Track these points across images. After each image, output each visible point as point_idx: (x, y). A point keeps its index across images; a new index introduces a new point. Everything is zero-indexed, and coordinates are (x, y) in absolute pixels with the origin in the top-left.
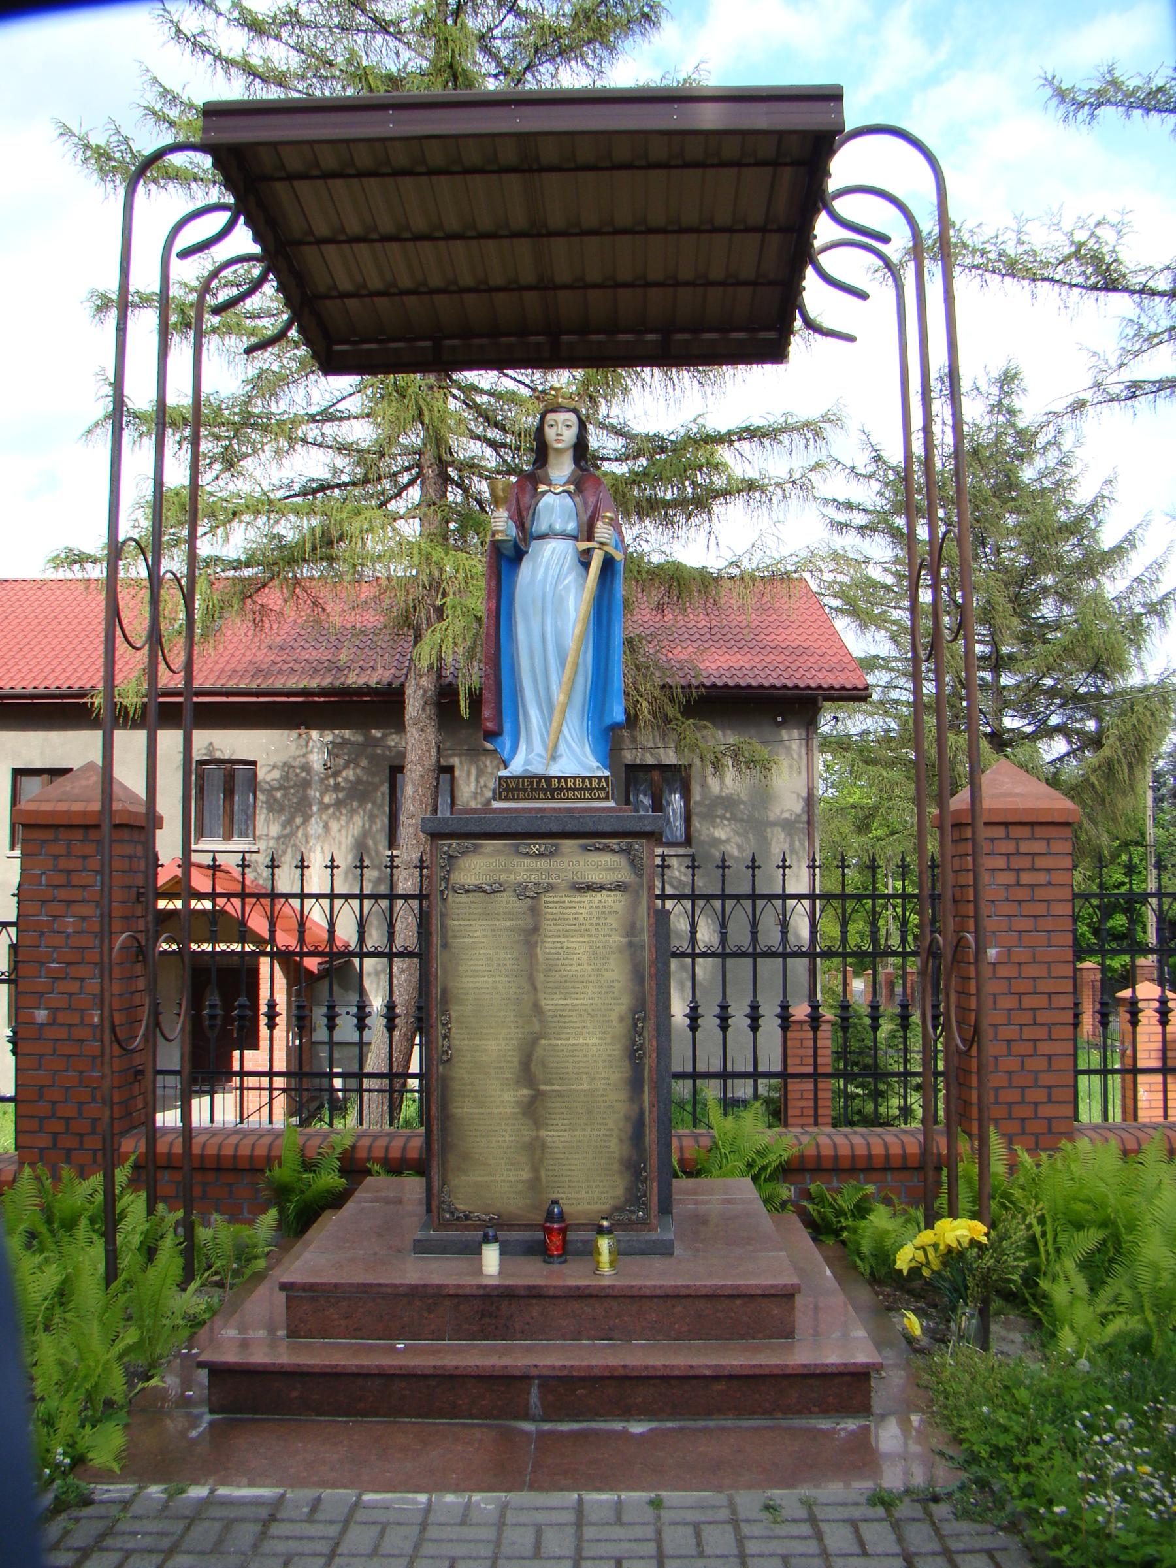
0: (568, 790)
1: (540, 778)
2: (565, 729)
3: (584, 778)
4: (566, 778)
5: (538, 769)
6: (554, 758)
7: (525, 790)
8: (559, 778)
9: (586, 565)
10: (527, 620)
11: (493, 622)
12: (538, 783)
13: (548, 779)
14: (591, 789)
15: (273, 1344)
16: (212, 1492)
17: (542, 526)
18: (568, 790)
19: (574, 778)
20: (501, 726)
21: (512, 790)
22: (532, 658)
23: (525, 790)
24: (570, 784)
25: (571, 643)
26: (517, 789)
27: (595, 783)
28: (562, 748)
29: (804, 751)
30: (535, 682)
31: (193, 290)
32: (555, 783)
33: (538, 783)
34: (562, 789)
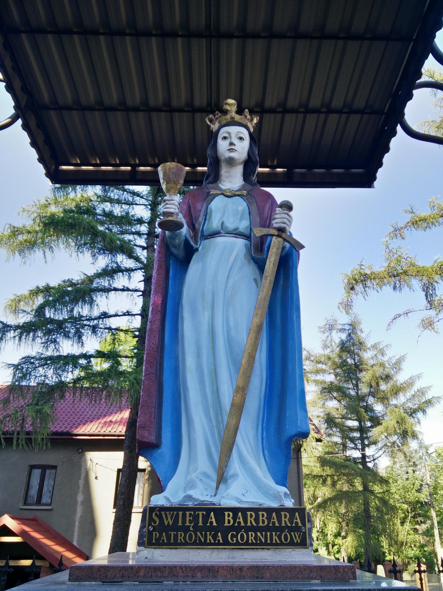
0: (248, 529)
1: (209, 510)
2: (239, 439)
3: (269, 511)
4: (244, 511)
5: (202, 494)
6: (222, 478)
7: (185, 529)
8: (235, 511)
9: (260, 266)
10: (194, 312)
11: (159, 317)
12: (206, 518)
13: (220, 512)
14: (281, 529)
15: (165, 214)
16: (7, 563)
17: (215, 223)
18: (248, 529)
19: (256, 510)
20: (159, 436)
21: (168, 529)
22: (199, 355)
23: (185, 529)
24: (251, 521)
25: (243, 337)
26: (175, 527)
27: (285, 521)
28: (235, 465)
29: (233, 333)
30: (202, 382)
31: (123, 274)
32: (228, 518)
33: (206, 518)
34: (238, 529)
